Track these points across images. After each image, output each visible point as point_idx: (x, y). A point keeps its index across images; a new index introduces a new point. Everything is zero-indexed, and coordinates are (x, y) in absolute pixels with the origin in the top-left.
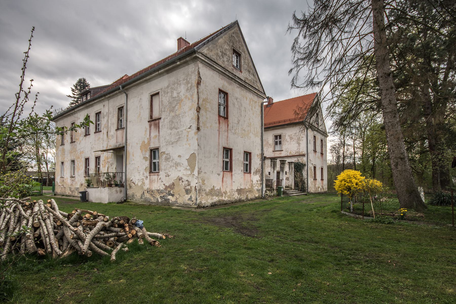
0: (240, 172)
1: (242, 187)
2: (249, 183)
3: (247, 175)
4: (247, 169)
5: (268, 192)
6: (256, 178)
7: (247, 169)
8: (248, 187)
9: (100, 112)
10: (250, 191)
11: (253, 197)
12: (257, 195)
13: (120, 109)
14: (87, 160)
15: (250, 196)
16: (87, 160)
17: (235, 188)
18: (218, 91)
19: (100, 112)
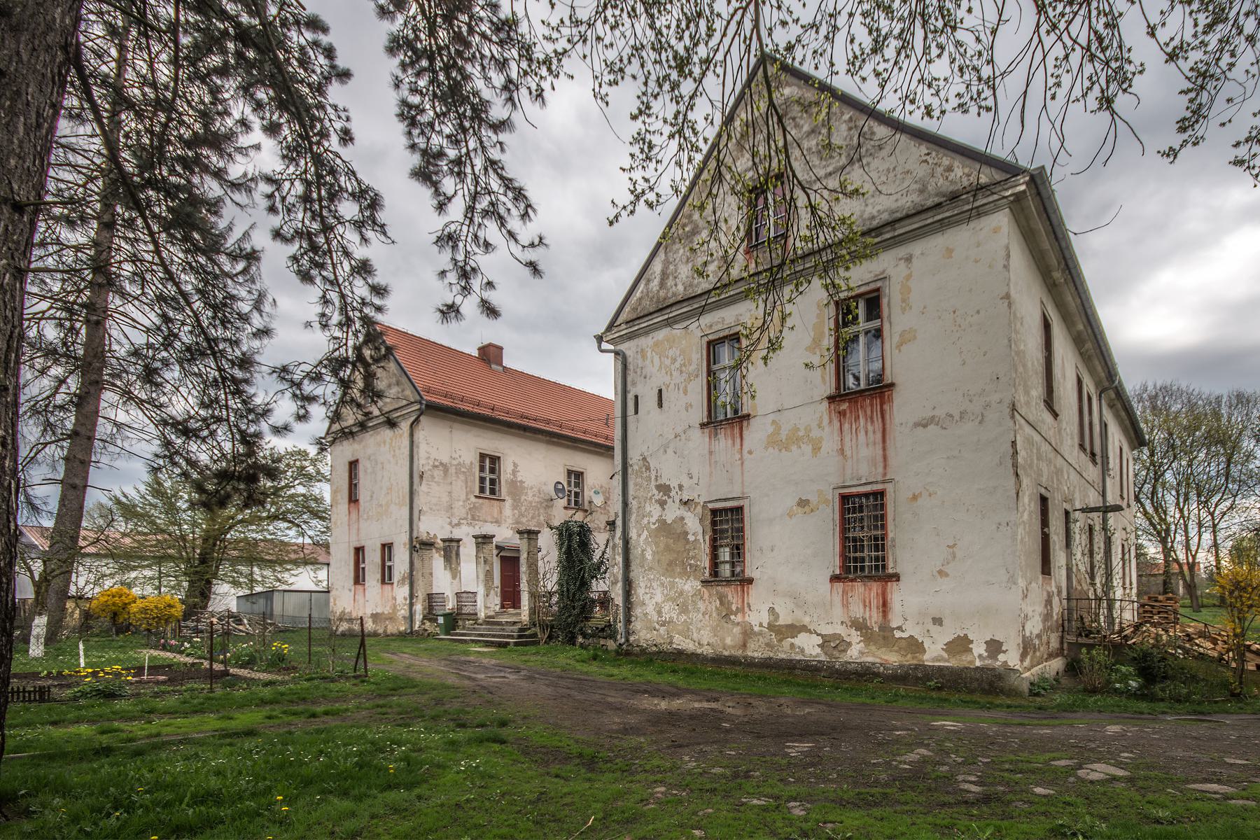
0: (375, 583)
1: (379, 611)
2: (390, 604)
3: (388, 588)
4: (386, 576)
5: (428, 624)
6: (402, 592)
7: (386, 576)
8: (387, 610)
9: (357, 461)
10: (391, 618)
11: (395, 631)
12: (402, 628)
13: (353, 465)
14: (359, 551)
15: (391, 629)
16: (359, 551)
17: (369, 612)
18: (439, 315)
19: (357, 461)
